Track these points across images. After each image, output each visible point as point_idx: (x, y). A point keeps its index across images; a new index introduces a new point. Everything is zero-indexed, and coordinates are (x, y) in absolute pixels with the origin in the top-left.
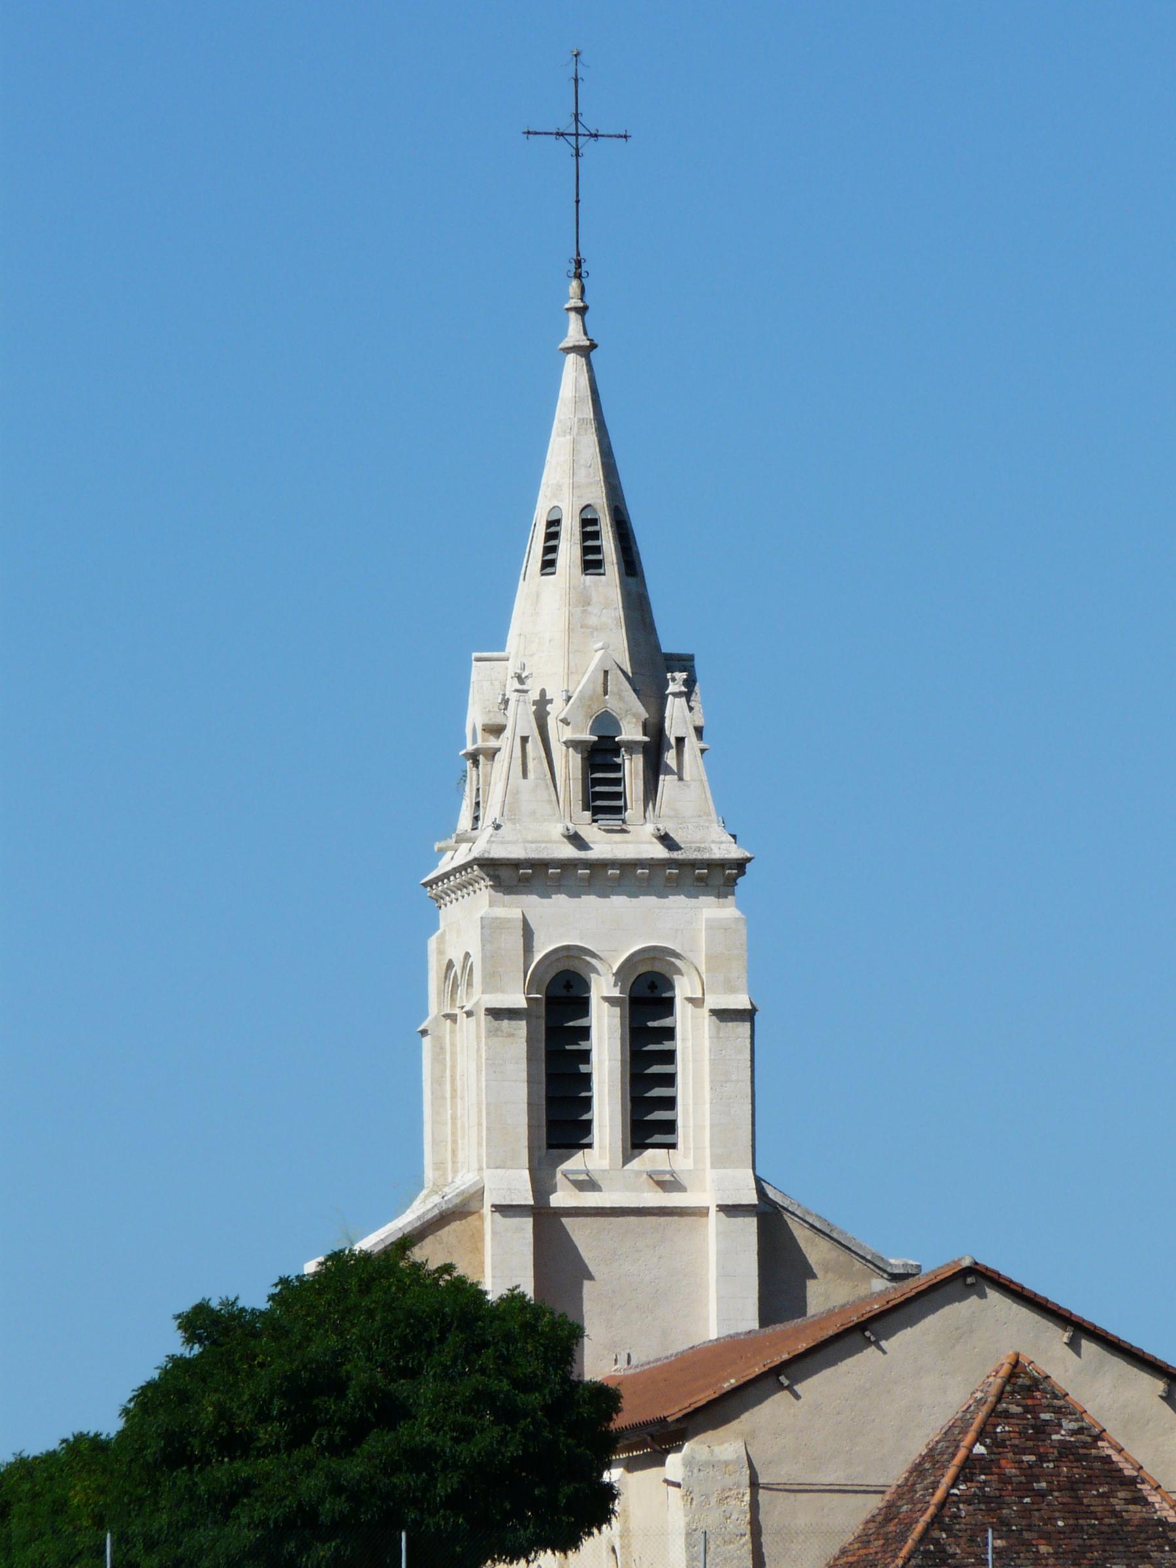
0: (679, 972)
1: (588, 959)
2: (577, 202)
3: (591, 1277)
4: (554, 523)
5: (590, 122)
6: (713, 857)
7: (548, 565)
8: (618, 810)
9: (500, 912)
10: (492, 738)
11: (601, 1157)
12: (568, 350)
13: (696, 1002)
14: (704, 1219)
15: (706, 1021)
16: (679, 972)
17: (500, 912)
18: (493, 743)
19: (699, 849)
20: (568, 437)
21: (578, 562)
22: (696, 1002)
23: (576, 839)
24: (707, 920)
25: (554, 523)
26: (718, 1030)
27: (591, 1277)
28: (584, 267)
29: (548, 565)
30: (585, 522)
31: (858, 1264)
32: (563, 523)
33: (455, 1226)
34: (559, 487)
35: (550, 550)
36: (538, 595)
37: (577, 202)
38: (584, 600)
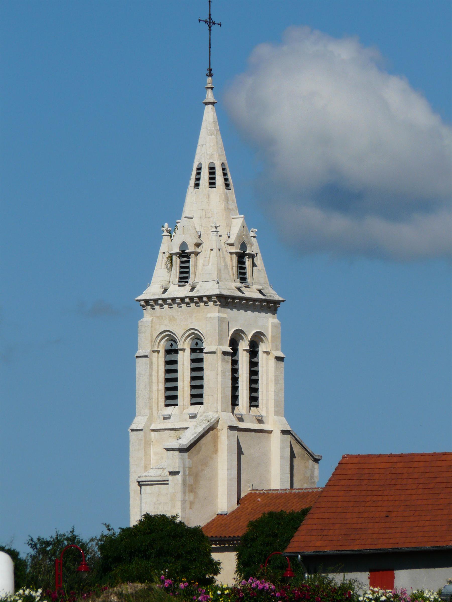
0: (242, 339)
1: (262, 337)
2: (210, 47)
3: (243, 454)
4: (199, 169)
5: (214, 19)
6: (274, 299)
7: (197, 185)
8: (187, 278)
9: (222, 315)
10: (197, 248)
11: (243, 410)
12: (207, 104)
13: (267, 353)
14: (270, 435)
15: (272, 362)
16: (242, 339)
17: (222, 315)
18: (198, 250)
19: (270, 296)
20: (213, 136)
21: (224, 185)
22: (267, 353)
23: (239, 289)
24: (272, 323)
25: (199, 169)
26: (277, 364)
27: (243, 454)
28: (212, 72)
29: (197, 185)
30: (210, 168)
31: (306, 455)
32: (216, 168)
33: (211, 432)
34: (212, 155)
35: (198, 179)
36: (209, 195)
37: (210, 47)
38: (227, 199)
